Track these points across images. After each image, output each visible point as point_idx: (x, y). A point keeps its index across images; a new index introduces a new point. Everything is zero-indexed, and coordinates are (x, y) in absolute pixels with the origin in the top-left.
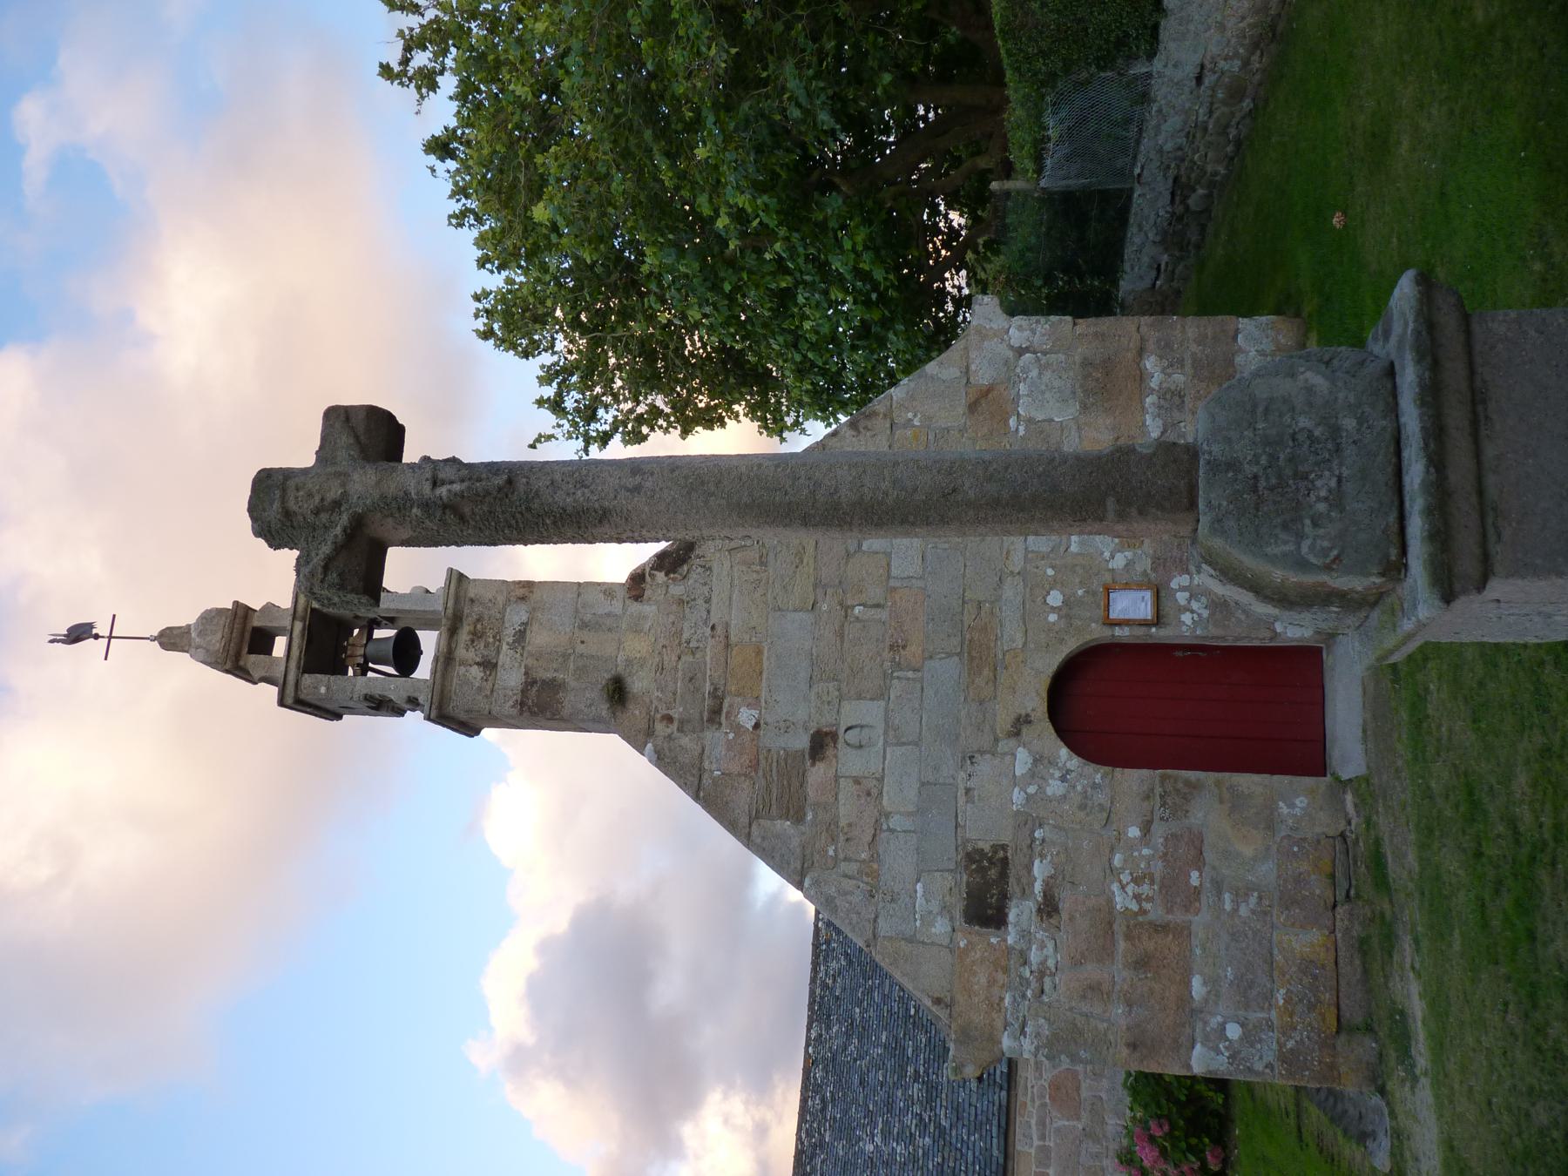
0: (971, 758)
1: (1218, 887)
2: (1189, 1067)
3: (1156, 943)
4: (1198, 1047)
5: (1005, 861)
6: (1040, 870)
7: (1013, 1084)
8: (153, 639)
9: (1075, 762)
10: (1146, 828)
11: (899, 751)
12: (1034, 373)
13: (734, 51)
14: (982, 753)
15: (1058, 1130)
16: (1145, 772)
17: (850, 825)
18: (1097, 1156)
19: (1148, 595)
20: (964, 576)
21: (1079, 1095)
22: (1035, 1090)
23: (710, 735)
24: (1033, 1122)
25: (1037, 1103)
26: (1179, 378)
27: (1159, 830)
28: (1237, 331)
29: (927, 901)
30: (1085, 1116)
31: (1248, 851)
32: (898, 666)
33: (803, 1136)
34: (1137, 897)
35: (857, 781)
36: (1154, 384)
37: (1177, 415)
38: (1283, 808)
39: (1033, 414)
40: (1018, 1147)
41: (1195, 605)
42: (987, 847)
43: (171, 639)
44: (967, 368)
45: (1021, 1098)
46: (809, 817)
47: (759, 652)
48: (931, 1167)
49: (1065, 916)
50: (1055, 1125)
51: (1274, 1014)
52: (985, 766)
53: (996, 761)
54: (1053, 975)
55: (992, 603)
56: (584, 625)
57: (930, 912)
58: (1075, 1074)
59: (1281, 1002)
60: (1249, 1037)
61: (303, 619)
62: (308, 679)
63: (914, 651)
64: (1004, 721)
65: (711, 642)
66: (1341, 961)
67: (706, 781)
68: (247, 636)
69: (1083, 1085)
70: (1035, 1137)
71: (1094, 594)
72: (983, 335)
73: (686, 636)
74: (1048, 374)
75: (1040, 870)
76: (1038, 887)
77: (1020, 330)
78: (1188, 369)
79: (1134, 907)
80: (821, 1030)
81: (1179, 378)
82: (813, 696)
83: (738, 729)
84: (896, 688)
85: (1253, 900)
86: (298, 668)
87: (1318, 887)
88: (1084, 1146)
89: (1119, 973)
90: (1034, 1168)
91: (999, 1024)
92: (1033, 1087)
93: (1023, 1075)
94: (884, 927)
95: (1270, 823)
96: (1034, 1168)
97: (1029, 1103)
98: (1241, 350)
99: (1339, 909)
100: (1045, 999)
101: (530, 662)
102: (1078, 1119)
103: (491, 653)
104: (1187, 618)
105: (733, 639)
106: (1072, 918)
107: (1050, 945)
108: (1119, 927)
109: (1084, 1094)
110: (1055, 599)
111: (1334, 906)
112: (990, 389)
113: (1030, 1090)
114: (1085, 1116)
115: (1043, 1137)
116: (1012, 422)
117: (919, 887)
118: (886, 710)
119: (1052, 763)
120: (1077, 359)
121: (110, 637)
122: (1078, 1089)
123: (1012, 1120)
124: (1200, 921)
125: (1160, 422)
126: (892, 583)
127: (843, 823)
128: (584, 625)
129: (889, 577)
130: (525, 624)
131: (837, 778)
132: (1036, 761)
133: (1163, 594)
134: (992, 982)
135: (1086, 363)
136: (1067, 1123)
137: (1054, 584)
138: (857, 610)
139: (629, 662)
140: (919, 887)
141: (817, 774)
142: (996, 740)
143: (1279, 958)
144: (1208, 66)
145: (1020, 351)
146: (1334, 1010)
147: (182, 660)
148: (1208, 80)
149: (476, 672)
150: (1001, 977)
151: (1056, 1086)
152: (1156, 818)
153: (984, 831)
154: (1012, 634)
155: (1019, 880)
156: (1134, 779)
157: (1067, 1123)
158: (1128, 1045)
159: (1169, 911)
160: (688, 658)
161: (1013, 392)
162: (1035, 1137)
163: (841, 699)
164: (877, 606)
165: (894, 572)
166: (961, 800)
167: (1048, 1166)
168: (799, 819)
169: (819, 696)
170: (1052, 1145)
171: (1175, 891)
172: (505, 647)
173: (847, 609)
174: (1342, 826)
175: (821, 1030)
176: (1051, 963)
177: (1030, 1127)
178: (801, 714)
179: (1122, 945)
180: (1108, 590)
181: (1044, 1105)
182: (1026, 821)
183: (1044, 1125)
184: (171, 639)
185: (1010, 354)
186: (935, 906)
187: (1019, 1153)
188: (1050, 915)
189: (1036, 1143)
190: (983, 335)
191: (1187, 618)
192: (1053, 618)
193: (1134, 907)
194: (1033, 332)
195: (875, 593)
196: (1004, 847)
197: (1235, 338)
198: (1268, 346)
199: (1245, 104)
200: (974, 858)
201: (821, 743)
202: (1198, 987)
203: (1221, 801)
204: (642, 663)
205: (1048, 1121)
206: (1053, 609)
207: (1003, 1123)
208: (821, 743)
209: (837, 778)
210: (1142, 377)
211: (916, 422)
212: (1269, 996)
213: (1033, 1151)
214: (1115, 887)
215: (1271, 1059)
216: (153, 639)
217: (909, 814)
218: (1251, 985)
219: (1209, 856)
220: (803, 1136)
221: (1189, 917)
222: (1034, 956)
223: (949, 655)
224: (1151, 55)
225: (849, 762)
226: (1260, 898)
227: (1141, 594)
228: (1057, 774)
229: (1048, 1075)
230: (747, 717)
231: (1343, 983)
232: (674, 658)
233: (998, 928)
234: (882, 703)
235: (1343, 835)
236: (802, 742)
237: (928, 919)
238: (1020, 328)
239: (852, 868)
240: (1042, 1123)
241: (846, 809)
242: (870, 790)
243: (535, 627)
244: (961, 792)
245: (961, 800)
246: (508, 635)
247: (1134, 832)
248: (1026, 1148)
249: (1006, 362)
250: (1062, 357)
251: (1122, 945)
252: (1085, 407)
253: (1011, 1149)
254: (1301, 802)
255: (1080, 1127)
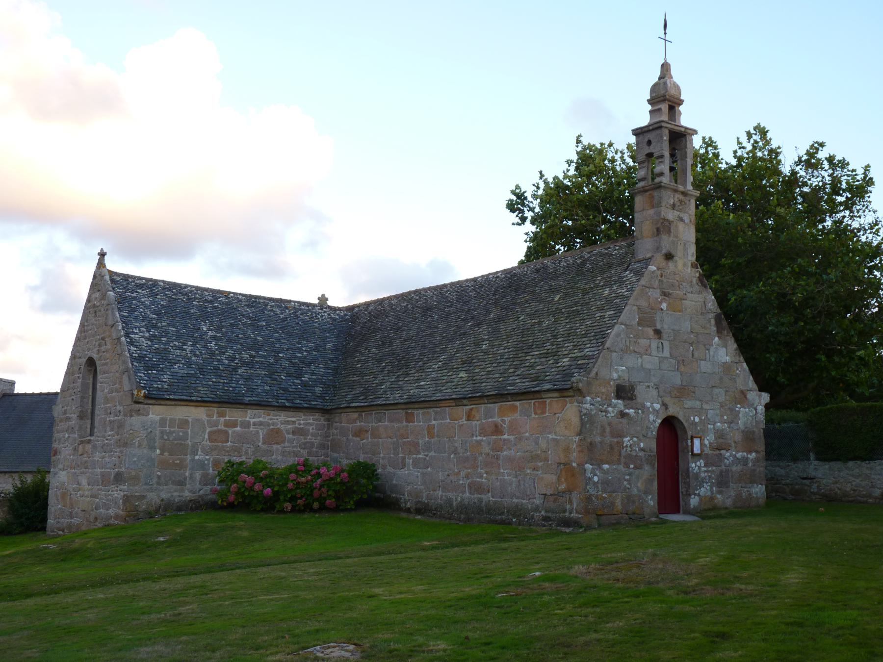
0: (657, 388)
1: (630, 474)
2: (654, 456)
3: (708, 440)
4: (591, 467)
5: (633, 400)
6: (631, 411)
7: (280, 409)
8: (665, 61)
9: (657, 425)
10: (642, 450)
11: (658, 361)
12: (751, 414)
13: (797, 304)
14: (658, 392)
15: (258, 432)
16: (655, 450)
17: (638, 343)
18: (247, 453)
19: (699, 452)
20: (701, 387)
21: (274, 444)
22: (275, 421)
23: (658, 291)
24: (261, 419)
25: (270, 422)
26: (750, 464)
27: (641, 454)
28: (762, 485)
29: (621, 371)
30: (264, 447)
31: (639, 484)
32: (678, 363)
33: (189, 288)
34: (627, 446)
35: (650, 346)
36: (749, 456)
37: (742, 463)
38: (650, 497)
39: (741, 413)
40: (249, 411)
41: (697, 468)
42: (635, 393)
43: (665, 68)
44: (751, 391)
45: (272, 413)
46: (640, 328)
47: (680, 311)
48: (359, 365)
49: (621, 420)
50: (260, 431)
51: (600, 493)
52: (654, 393)
53: (656, 397)
54: (605, 416)
55: (694, 397)
56: (685, 244)
57: (618, 372)
58: (283, 442)
59: (604, 495)
60: (595, 483)
61: (684, 132)
62: (667, 132)
63: (682, 368)
64: (667, 400)
65: (682, 293)
66: (615, 516)
67: (647, 290)
68: (673, 104)
69: (279, 446)
70: (254, 420)
71: (698, 433)
72: (760, 396)
73: (683, 283)
74: (750, 418)
75: (631, 411)
76: (627, 411)
77: (761, 409)
78: (753, 468)
79: (625, 445)
80: (244, 302)
81: (750, 464)
82: (670, 331)
83: (661, 302)
84: (673, 361)
85: (628, 486)
86: (672, 129)
87: (631, 509)
88: (252, 446)
89: (608, 439)
90: (240, 419)
91: (593, 396)
92: (277, 419)
93: (282, 414)
94: (614, 354)
95: (646, 492)
96: (240, 419)
97: (270, 417)
98: (758, 486)
99: (626, 516)
100: (600, 413)
101: (675, 223)
102: (264, 443)
103: (676, 208)
104: (694, 465)
105: (683, 301)
106: (621, 423)
107: (613, 415)
108: (619, 439)
109: (275, 446)
110: (697, 419)
111: (627, 514)
112: (746, 397)
113: (276, 417)
114: (264, 447)
115: (254, 424)
116: (739, 406)
117: (624, 368)
118: (667, 358)
119: (657, 417)
120: (754, 429)
121: (665, 40)
122: (277, 443)
123: (262, 408)
124: (621, 467)
125: (740, 457)
126: (699, 361)
127: (639, 340)
128: (685, 244)
129: (701, 360)
130: (684, 221)
131: (650, 339)
132: (657, 411)
133: (698, 457)
134: (603, 393)
135: (754, 432)
136: (261, 437)
137: (700, 419)
138: (691, 348)
139: (676, 262)
140: (624, 368)
141: (650, 331)
142: (661, 397)
143: (614, 494)
144: (815, 481)
145: (756, 409)
146: (602, 513)
147: (658, 73)
148: (807, 482)
149: (671, 202)
150: (604, 397)
151: (278, 432)
152: (646, 453)
153: (640, 391)
154: (689, 404)
155: (628, 404)
156: (653, 445)
157: (261, 437)
158: (591, 442)
159: (624, 457)
160: (677, 284)
161: (746, 406)
162: (254, 420)
163: (669, 341)
164: (693, 355)
165: (702, 362)
166: (647, 384)
167: (241, 427)
168: (639, 324)
169: (670, 333)
170: (251, 429)
171: (630, 458)
172: (678, 213)
173: (691, 344)
174: (647, 517)
175: (244, 302)
176: (609, 415)
177: (259, 418)
178: (666, 326)
179: (616, 440)
180: (700, 438)
181: (269, 425)
182: (643, 407)
183: (260, 425)
184: (665, 68)
185: (755, 406)
186: (620, 373)
187: (246, 412)
188: (621, 415)
189: (252, 421)
190: (760, 396)
191: (694, 465)
192: (692, 418)
193: (625, 445)
194: (761, 414)
195: (696, 354)
196: (636, 399)
197: (761, 484)
198: (759, 495)
199: (791, 496)
200: (632, 388)
201: (658, 333)
202: (606, 466)
203: (651, 476)
204: (676, 266)
205: (262, 427)
206: (694, 418)
207: (263, 403)
208: (658, 333)
209: (650, 339)
210: (750, 452)
211: (738, 372)
212: (604, 491)
213: (248, 419)
214: (628, 438)
215: (590, 492)
216: (665, 61)
217: (642, 365)
218: (608, 485)
219: (637, 471)
220: (189, 288)
221: (622, 464)
222: (610, 409)
223: (682, 381)
224: (817, 459)
225: (654, 344)
226: (629, 489)
227: (699, 449)
228: (655, 419)
229: (282, 427)
230: (664, 306)
231: (609, 516)
232: (677, 279)
233: (616, 396)
234: (669, 356)
235: (644, 517)
236: (659, 327)
237: (617, 371)
238: (762, 410)
239: (628, 344)
240: (261, 424)
241: (643, 342)
242: (647, 351)
243: (683, 225)
244: (649, 384)
245: (647, 384)
246: (682, 215)
247: (642, 445)
248: (249, 415)
249: (753, 404)
250: (754, 424)
251: (616, 440)
252: (743, 431)
253: (249, 407)
254: (652, 503)
255: (260, 444)
